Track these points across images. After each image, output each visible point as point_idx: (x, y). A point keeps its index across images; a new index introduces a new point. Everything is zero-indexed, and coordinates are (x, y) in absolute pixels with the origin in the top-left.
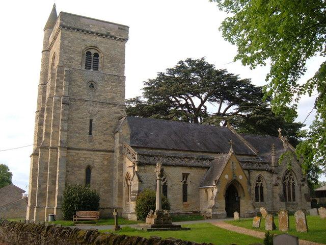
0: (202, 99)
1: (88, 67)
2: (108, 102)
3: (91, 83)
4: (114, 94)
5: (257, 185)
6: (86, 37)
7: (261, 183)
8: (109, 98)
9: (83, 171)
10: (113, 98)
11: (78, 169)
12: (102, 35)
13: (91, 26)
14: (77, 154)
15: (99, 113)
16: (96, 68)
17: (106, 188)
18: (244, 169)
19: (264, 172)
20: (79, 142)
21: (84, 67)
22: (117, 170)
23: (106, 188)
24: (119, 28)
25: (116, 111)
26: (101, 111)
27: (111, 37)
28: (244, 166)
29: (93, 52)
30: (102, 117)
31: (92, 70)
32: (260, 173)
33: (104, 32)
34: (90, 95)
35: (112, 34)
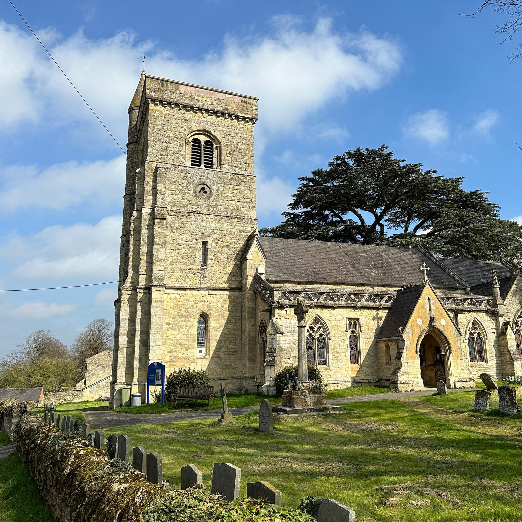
0: (406, 224)
1: (196, 163)
2: (229, 214)
3: (202, 186)
4: (238, 203)
5: (471, 334)
6: (190, 115)
7: (477, 331)
8: (231, 210)
9: (194, 323)
10: (237, 209)
11: (183, 319)
12: (215, 113)
13: (196, 98)
14: (183, 295)
15: (215, 231)
16: (209, 165)
17: (230, 346)
18: (449, 310)
19: (481, 314)
20: (185, 278)
21: (190, 163)
22: (247, 317)
23: (230, 346)
24: (242, 101)
25: (243, 229)
26: (352, 432)
27: (230, 115)
28: (449, 305)
29: (203, 138)
30: (221, 239)
31: (202, 167)
32: (474, 315)
33: (219, 108)
34: (201, 205)
35: (232, 110)
